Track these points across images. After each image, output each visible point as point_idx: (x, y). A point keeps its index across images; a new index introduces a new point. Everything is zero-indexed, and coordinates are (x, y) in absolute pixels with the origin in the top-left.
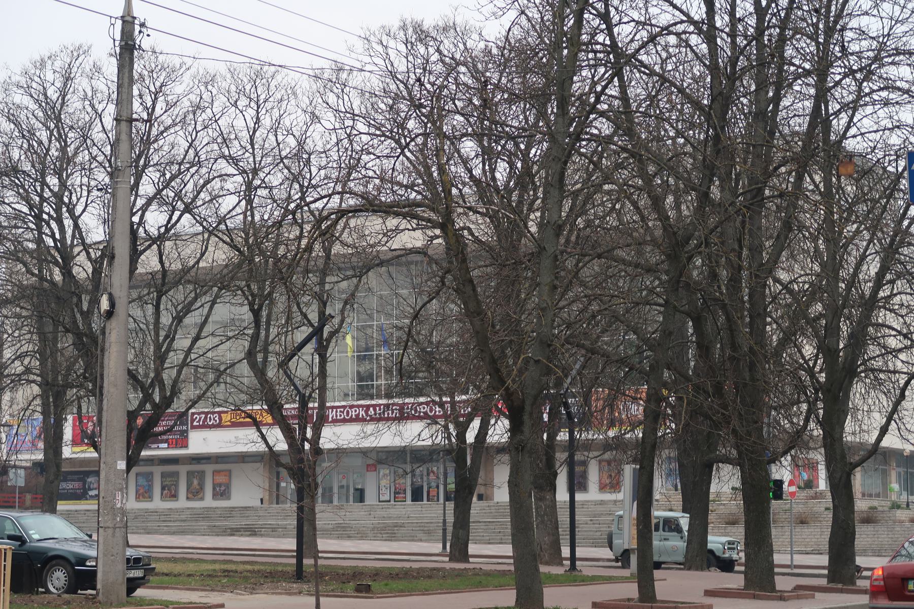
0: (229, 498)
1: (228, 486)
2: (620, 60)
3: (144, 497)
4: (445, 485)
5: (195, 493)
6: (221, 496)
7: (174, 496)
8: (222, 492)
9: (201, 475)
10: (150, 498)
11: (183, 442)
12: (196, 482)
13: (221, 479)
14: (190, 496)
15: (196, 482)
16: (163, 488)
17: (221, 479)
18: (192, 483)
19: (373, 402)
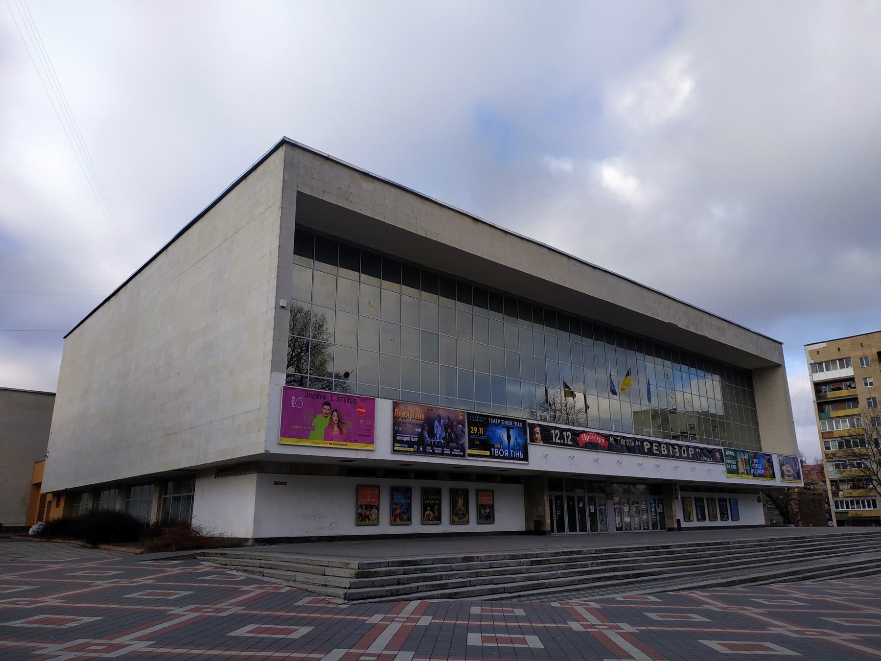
0: (493, 522)
1: (492, 507)
2: (759, 501)
3: (401, 520)
4: (341, 612)
5: (432, 513)
6: (487, 519)
7: (438, 519)
8: (487, 516)
9: (407, 492)
10: (717, 520)
11: (736, 517)
12: (460, 502)
13: (485, 500)
14: (456, 519)
15: (460, 502)
16: (424, 510)
17: (485, 500)
18: (457, 503)
19: (688, 444)
